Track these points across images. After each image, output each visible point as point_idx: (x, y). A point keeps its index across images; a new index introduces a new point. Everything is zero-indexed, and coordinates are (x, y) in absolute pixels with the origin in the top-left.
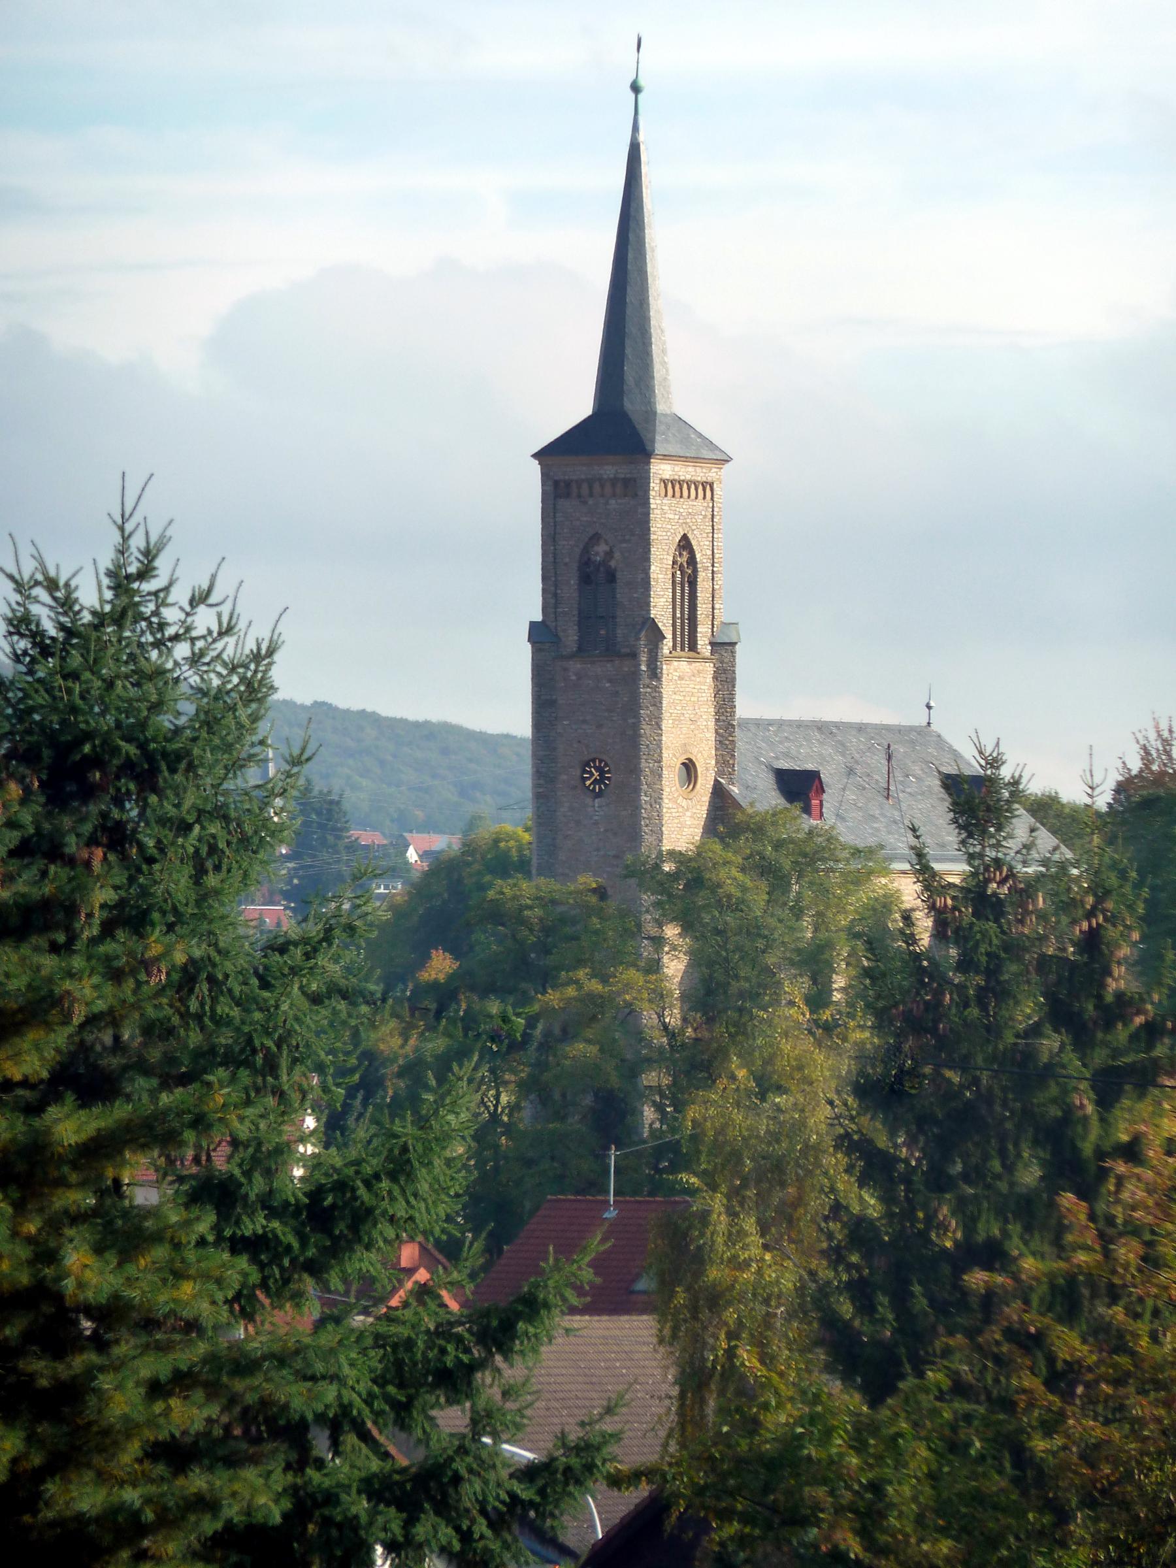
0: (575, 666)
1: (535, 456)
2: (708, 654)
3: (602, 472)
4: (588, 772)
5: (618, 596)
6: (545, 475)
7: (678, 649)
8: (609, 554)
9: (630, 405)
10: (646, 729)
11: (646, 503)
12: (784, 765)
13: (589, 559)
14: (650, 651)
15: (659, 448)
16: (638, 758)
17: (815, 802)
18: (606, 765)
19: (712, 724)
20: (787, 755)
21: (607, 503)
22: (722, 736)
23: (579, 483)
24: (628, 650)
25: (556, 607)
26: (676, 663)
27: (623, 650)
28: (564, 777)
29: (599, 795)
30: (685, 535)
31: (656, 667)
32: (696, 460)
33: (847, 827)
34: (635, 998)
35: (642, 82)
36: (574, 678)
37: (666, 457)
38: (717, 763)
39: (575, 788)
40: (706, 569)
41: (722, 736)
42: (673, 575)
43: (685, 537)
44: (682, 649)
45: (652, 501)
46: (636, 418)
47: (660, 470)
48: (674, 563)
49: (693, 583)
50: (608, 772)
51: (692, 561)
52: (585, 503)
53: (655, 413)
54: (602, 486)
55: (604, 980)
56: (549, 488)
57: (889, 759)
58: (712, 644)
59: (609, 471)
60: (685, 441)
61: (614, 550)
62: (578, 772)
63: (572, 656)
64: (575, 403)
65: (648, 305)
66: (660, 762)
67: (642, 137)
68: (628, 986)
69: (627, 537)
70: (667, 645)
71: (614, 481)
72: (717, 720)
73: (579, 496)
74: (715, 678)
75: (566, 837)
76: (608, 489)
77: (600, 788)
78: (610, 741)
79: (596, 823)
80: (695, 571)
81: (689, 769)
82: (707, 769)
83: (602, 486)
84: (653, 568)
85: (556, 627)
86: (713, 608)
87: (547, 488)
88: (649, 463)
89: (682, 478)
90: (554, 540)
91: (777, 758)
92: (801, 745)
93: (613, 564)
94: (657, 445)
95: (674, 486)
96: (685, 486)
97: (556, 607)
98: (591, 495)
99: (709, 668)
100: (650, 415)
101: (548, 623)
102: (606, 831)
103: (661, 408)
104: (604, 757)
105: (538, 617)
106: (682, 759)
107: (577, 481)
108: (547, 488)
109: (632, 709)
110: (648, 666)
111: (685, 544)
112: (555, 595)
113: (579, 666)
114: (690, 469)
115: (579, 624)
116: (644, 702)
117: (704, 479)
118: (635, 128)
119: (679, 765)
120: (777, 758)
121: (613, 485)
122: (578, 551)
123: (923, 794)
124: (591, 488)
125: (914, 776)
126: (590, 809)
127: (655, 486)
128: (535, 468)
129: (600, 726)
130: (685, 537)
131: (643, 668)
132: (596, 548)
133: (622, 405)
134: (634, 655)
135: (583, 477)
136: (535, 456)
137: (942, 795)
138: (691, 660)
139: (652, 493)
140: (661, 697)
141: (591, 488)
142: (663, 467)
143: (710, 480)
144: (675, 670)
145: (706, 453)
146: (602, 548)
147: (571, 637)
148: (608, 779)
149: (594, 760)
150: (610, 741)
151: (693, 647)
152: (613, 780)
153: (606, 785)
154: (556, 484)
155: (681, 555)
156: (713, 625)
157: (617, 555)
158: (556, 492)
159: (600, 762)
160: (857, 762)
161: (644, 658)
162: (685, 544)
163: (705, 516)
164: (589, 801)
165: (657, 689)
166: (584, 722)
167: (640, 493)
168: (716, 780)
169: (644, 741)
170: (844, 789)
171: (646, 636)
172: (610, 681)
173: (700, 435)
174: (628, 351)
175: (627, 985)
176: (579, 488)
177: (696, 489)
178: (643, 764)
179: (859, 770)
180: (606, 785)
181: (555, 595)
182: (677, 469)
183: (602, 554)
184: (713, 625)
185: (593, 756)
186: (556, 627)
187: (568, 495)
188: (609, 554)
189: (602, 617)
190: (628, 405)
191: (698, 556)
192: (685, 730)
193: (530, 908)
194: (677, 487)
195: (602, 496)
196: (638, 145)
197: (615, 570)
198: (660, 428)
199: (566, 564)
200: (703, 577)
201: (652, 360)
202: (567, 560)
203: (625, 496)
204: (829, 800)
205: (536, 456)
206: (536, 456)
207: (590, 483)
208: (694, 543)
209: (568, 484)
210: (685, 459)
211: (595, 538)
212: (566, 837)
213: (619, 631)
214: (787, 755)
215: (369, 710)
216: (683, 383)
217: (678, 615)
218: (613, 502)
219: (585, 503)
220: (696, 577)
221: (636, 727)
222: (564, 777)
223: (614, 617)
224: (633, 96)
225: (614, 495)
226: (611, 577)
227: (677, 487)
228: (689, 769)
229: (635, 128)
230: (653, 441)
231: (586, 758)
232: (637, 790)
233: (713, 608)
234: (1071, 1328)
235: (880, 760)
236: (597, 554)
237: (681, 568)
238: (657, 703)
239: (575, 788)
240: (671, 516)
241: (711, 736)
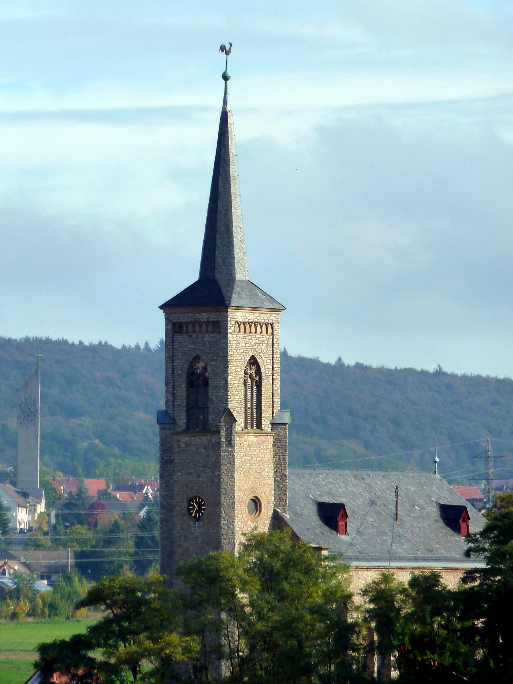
0: (185, 438)
2: (269, 430)
3: (201, 317)
5: (210, 395)
6: (167, 320)
7: (249, 428)
8: (205, 369)
9: (220, 277)
10: (224, 478)
11: (226, 337)
12: (326, 499)
13: (193, 371)
14: (227, 429)
15: (234, 302)
16: (220, 496)
17: (341, 524)
19: (272, 474)
20: (329, 493)
21: (203, 337)
22: (279, 482)
23: (187, 324)
24: (215, 429)
25: (173, 401)
26: (246, 437)
27: (213, 429)
29: (198, 519)
30: (253, 356)
31: (231, 440)
32: (261, 309)
33: (364, 539)
34: (173, 652)
35: (229, 73)
36: (184, 446)
37: (239, 308)
38: (275, 499)
39: (184, 515)
40: (268, 377)
41: (279, 482)
42: (245, 382)
43: (253, 358)
44: (252, 428)
45: (229, 335)
46: (222, 283)
47: (235, 316)
48: (246, 373)
49: (259, 386)
50: (204, 505)
51: (258, 372)
52: (190, 336)
53: (234, 280)
54: (201, 326)
55: (155, 640)
56: (170, 328)
57: (397, 495)
58: (272, 424)
59: (204, 317)
60: (254, 297)
61: (207, 366)
62: (186, 505)
64: (187, 273)
65: (232, 212)
66: (234, 499)
67: (229, 108)
68: (169, 644)
69: (215, 358)
70: (239, 426)
71: (207, 323)
72: (275, 472)
73: (187, 332)
74: (274, 445)
75: (179, 546)
76: (204, 327)
77: (199, 515)
78: (205, 485)
79: (197, 537)
80: (261, 378)
81: (256, 502)
82: (269, 503)
83: (201, 326)
84: (230, 377)
85: (174, 414)
86: (273, 402)
87: (169, 327)
88: (227, 312)
89: (251, 321)
90: (173, 360)
91: (321, 495)
92: (340, 487)
93: (207, 374)
94: (233, 301)
95: (245, 326)
96: (253, 325)
97: (173, 401)
98: (194, 332)
99: (270, 439)
100: (231, 280)
101: (169, 412)
102: (202, 542)
103: (239, 276)
104: (200, 495)
105: (164, 408)
106: (251, 496)
107: (186, 323)
108: (169, 327)
109: (217, 466)
110: (226, 438)
111: (253, 361)
112: (173, 394)
113: (186, 438)
114: (257, 315)
115: (187, 412)
116: (223, 461)
117: (267, 321)
118: (225, 102)
119: (248, 500)
120: (321, 495)
121: (207, 326)
122: (186, 366)
123: (423, 517)
124: (194, 326)
125: (418, 506)
126: (193, 529)
127: (232, 326)
128: (161, 315)
129: (199, 476)
130: (253, 358)
131: (223, 440)
132: (198, 365)
133: (214, 276)
134: (218, 432)
135: (189, 320)
137: (437, 518)
138: (256, 434)
139: (229, 330)
140: (234, 458)
141: (194, 326)
142: (237, 314)
143: (270, 321)
144: (246, 441)
145: (267, 305)
146: (201, 365)
147: (182, 421)
148: (204, 509)
150: (205, 485)
151: (259, 426)
152: (206, 511)
153: (202, 514)
154: (174, 324)
155: (251, 368)
156: (273, 412)
157: (209, 369)
158: (174, 328)
160: (378, 497)
161: (223, 434)
162: (253, 361)
163: (268, 344)
164: (192, 523)
165: (231, 454)
166: (190, 474)
167: (222, 331)
168: (275, 510)
169: (223, 485)
170: (366, 515)
171: (224, 420)
173: (265, 294)
174: (218, 241)
175: (168, 643)
176: (187, 327)
177: (261, 328)
178: (223, 500)
179: (379, 502)
180: (202, 514)
181: (173, 394)
182: (247, 315)
183: (201, 369)
184: (273, 412)
185: (195, 495)
186: (174, 414)
187: (180, 332)
188: (205, 369)
189: (201, 408)
190: (217, 276)
191: (262, 369)
192: (252, 479)
193: (119, 594)
194: (248, 326)
195: (201, 332)
196: (226, 113)
197: (208, 379)
198: (236, 289)
199: (179, 375)
200: (265, 382)
201: (233, 247)
202: (180, 372)
203: (214, 332)
204: (352, 524)
205: (162, 307)
206: (162, 307)
208: (259, 361)
209: (181, 324)
210: (253, 309)
211: (197, 359)
213: (210, 417)
214: (329, 493)
216: (248, 263)
217: (249, 406)
218: (206, 336)
220: (261, 382)
221: (219, 477)
223: (208, 408)
225: (207, 332)
226: (206, 384)
227: (248, 326)
228: (256, 502)
229: (225, 102)
230: (230, 298)
231: (191, 496)
232: (219, 516)
233: (273, 402)
235: (392, 496)
236: (198, 368)
237: (251, 376)
238: (232, 462)
239: (184, 515)
240: (243, 345)
241: (271, 482)
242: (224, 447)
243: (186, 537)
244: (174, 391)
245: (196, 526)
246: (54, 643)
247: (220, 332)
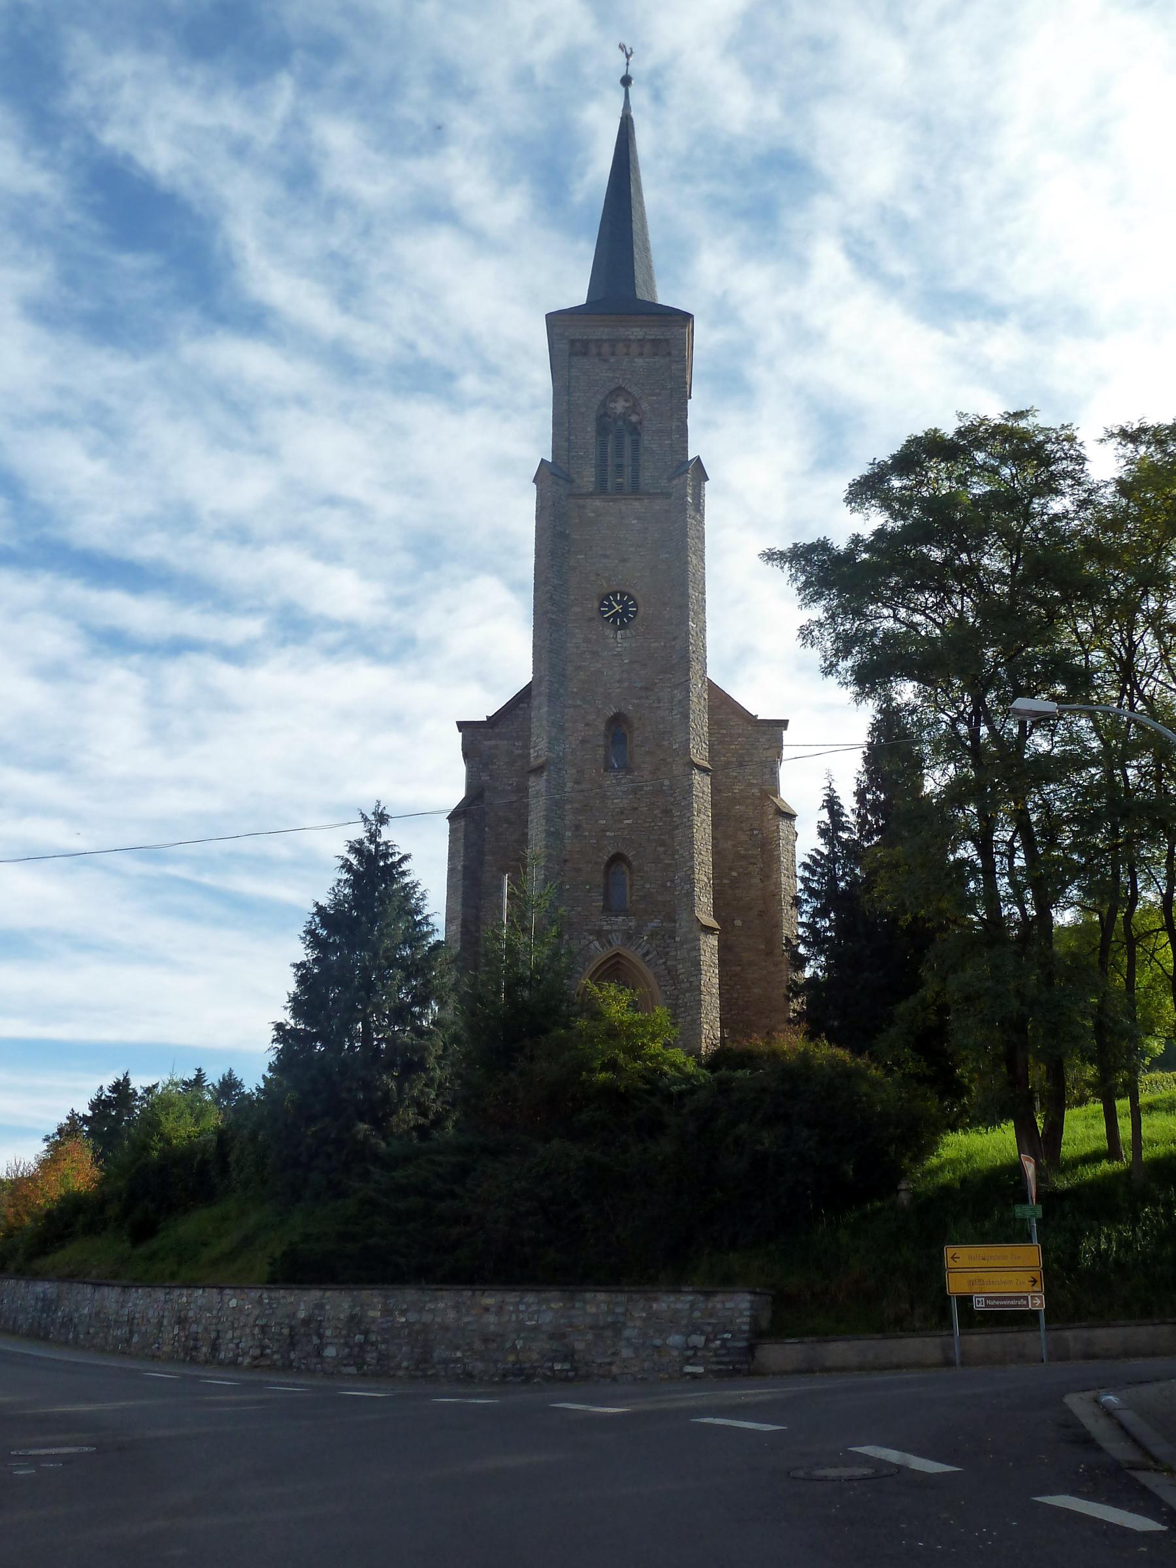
1: (462, 726)
4: (605, 606)
10: (693, 559)
14: (694, 487)
18: (629, 600)
23: (599, 342)
28: (577, 609)
39: (591, 619)
62: (596, 604)
63: (605, 341)
71: (641, 342)
73: (599, 354)
75: (579, 668)
79: (619, 655)
102: (631, 662)
110: (693, 489)
128: (762, 710)
136: (462, 726)
147: (588, 478)
149: (614, 594)
159: (622, 596)
164: (609, 633)
167: (674, 352)
172: (638, 519)
181: (568, 440)
203: (655, 354)
207: (613, 342)
209: (586, 343)
212: (579, 668)
215: (291, 986)
219: (606, 361)
222: (577, 609)
224: (623, 90)
225: (641, 354)
234: (902, 1174)
242: (691, 512)
243: (594, 653)
244: (570, 434)
245: (619, 636)
246: (302, 981)
247: (669, 354)
